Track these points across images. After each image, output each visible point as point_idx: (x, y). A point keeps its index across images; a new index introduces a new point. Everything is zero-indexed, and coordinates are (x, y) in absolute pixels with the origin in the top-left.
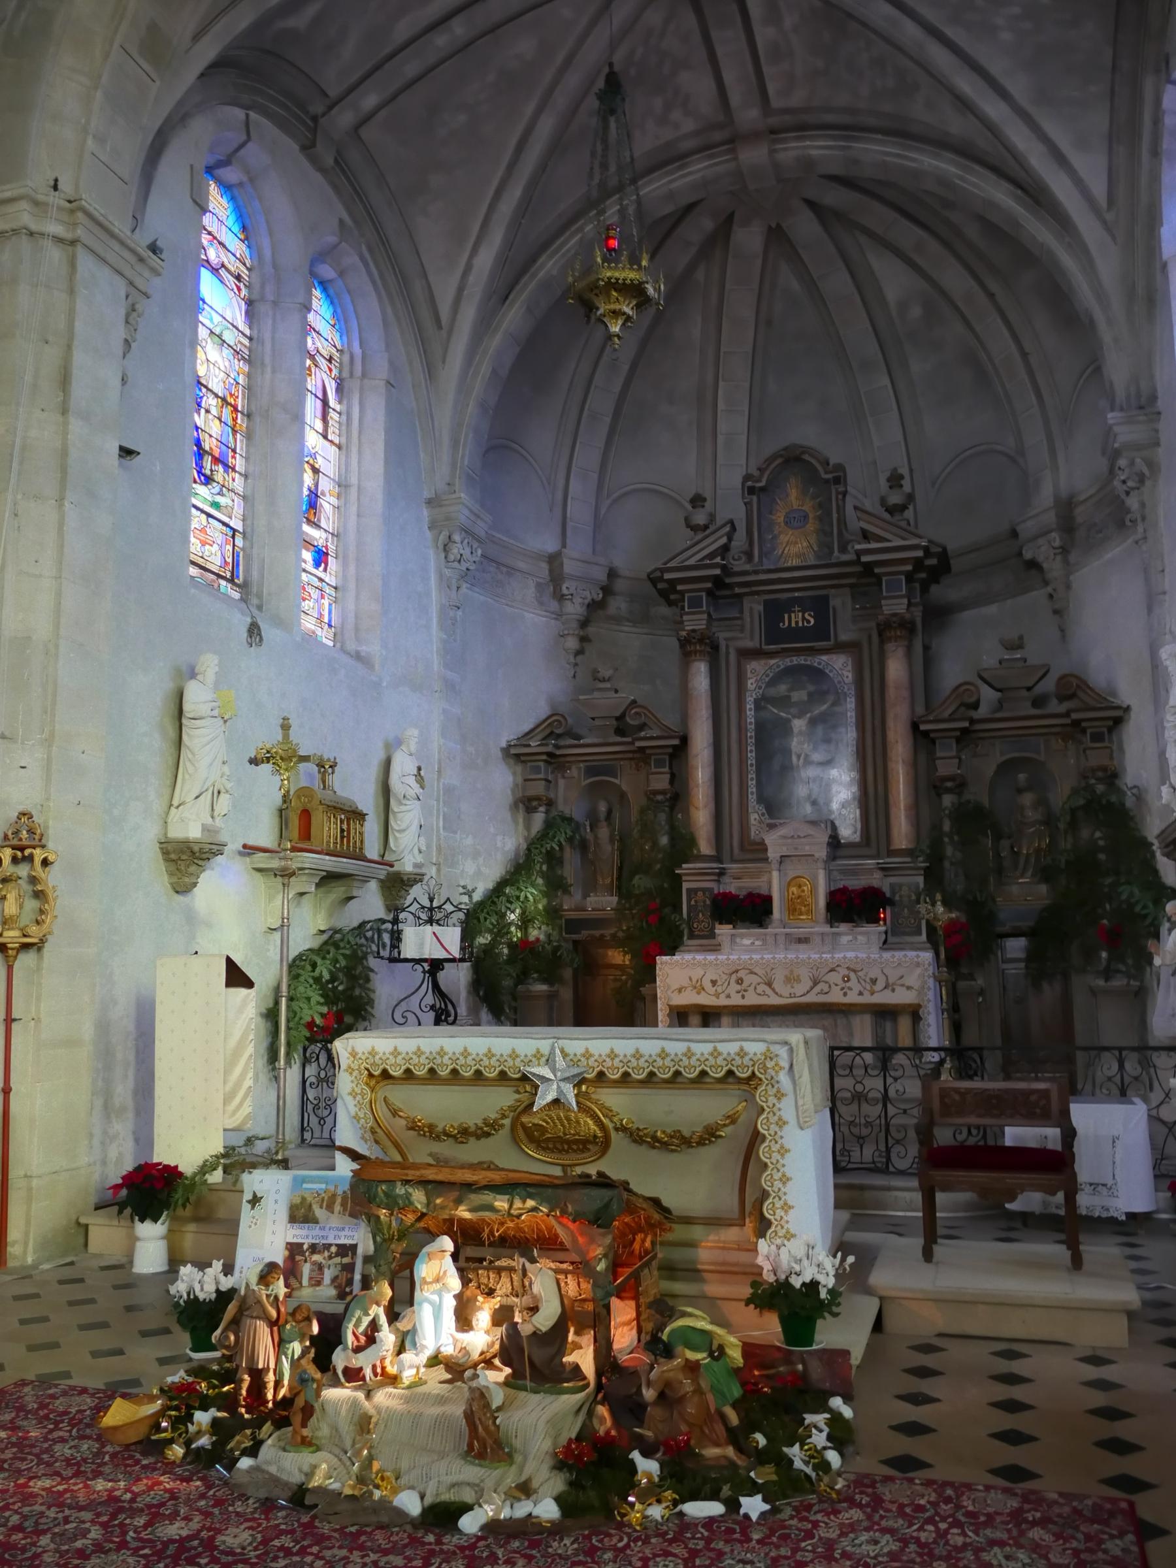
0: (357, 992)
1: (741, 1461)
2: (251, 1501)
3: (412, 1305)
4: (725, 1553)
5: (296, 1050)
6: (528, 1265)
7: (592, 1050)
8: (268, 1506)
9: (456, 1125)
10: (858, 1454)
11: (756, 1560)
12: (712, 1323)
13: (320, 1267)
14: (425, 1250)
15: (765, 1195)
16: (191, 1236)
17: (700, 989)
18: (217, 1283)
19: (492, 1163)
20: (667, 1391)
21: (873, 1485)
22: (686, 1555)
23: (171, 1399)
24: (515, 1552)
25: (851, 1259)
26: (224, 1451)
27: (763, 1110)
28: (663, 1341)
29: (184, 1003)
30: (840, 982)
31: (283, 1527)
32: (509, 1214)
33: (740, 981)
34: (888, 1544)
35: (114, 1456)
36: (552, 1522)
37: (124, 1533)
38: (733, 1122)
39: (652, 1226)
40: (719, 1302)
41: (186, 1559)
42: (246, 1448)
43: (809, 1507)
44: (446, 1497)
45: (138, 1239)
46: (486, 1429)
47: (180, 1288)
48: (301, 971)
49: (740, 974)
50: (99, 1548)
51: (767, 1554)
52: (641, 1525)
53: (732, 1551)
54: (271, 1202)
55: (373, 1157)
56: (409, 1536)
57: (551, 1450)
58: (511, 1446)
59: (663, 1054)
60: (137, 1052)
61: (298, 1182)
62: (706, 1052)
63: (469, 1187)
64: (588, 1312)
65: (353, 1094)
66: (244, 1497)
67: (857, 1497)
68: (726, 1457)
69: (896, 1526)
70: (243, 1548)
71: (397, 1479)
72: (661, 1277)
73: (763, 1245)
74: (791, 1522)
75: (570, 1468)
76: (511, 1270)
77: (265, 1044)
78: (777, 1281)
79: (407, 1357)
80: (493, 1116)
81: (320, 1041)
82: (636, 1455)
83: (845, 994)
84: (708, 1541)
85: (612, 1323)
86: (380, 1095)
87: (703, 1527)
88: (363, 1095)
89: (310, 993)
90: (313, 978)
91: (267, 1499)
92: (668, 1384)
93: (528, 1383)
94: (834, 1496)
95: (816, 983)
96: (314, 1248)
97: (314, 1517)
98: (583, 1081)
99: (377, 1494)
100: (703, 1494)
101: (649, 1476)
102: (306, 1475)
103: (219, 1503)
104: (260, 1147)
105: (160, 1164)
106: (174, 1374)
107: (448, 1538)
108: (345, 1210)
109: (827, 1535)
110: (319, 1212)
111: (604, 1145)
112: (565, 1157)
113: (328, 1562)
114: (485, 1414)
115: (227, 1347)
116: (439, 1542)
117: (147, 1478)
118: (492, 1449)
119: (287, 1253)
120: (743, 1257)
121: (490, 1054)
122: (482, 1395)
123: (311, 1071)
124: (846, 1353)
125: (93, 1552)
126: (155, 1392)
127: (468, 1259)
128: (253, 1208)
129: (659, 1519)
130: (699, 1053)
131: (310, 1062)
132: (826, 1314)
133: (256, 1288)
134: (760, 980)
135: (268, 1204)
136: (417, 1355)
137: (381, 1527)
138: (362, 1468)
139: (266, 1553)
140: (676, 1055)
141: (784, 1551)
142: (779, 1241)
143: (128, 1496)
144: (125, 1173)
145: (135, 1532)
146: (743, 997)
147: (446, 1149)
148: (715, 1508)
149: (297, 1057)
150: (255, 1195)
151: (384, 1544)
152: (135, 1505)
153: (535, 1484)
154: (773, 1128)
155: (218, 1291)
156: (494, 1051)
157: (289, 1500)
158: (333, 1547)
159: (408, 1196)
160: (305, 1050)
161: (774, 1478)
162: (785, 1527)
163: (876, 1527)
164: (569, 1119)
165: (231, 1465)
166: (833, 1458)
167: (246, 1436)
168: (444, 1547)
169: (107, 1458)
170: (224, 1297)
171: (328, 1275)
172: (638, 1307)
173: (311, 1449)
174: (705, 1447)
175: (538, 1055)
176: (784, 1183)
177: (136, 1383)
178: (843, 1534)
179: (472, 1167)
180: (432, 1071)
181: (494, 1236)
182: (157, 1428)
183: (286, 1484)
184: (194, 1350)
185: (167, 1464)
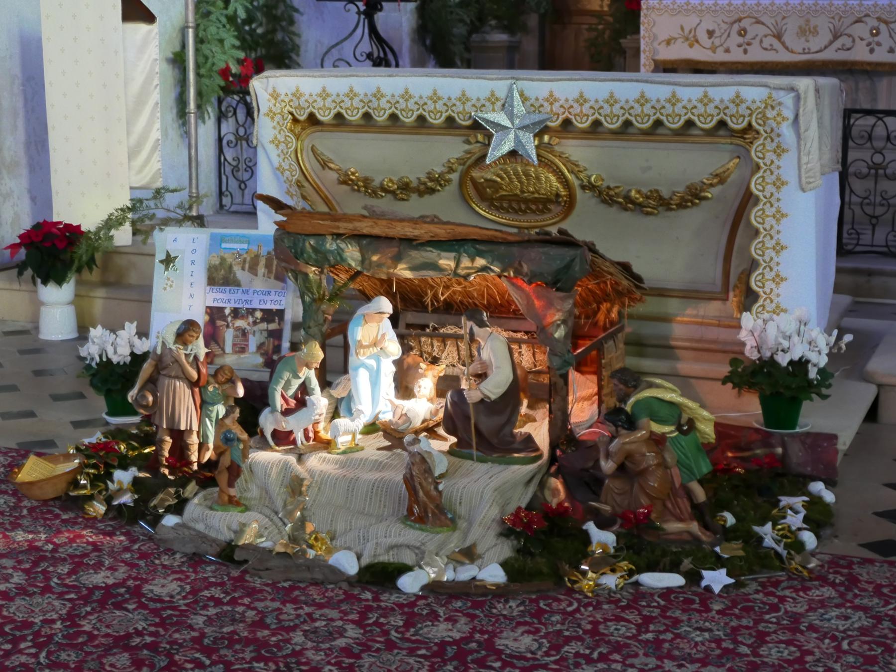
0: (279, 36)
1: (705, 537)
2: (178, 556)
3: (345, 371)
4: (682, 621)
5: (208, 101)
6: (476, 329)
7: (557, 94)
8: (196, 560)
9: (395, 179)
10: (836, 537)
11: (715, 628)
12: (682, 395)
13: (244, 333)
14: (360, 312)
15: (754, 264)
16: (99, 300)
17: (694, 41)
18: (132, 346)
19: (435, 217)
20: (627, 463)
21: (850, 566)
22: (640, 621)
23: (88, 457)
24: (457, 611)
25: (848, 338)
26: (147, 508)
27: (758, 168)
28: (626, 413)
29: (75, 39)
30: (867, 35)
31: (213, 580)
32: (455, 274)
33: (742, 33)
34: (859, 620)
35: (31, 510)
36: (498, 586)
37: (48, 579)
38: (722, 182)
39: (620, 295)
40: (693, 381)
41: (113, 604)
42: (170, 506)
43: (776, 584)
44: (384, 558)
45: (42, 304)
46: (427, 494)
47: (91, 350)
48: (212, 9)
49: (743, 24)
50: (22, 591)
51: (726, 624)
52: (592, 592)
53: (690, 619)
54: (187, 263)
55: (299, 208)
56: (345, 593)
57: (498, 518)
58: (455, 512)
59: (643, 100)
60: (26, 100)
61: (216, 241)
62: (694, 99)
63: (409, 242)
64: (544, 385)
65: (275, 142)
66: (170, 552)
67: (831, 577)
68: (689, 533)
69: (870, 604)
70: (172, 597)
71: (332, 539)
72: (628, 353)
73: (747, 320)
74: (756, 596)
75: (518, 536)
76: (457, 337)
77: (172, 95)
78: (759, 359)
79: (342, 422)
80: (439, 169)
81: (237, 93)
82: (590, 526)
83: (872, 51)
84: (664, 610)
85: (570, 398)
86: (307, 143)
87: (659, 597)
88: (286, 143)
89: (223, 34)
90: (226, 16)
91: (194, 554)
92: (629, 456)
93: (475, 452)
94: (805, 573)
95: (836, 37)
96: (236, 313)
97: (245, 572)
98: (545, 130)
99: (311, 553)
100: (662, 565)
101: (604, 546)
102: (235, 532)
103: (143, 556)
104: (171, 200)
105: (60, 223)
106: (91, 436)
107: (384, 597)
108: (270, 271)
109: (795, 610)
110: (241, 275)
111: (570, 205)
112: (522, 218)
113: (260, 612)
114: (426, 479)
115: (146, 407)
116: (376, 599)
117: (68, 531)
118: (434, 513)
119: (207, 318)
120: (724, 334)
121: (435, 97)
122: (423, 460)
123: (228, 127)
124: (832, 438)
125: (17, 594)
126: (71, 452)
127: (409, 326)
128: (167, 269)
129: (613, 587)
130: (686, 99)
131: (226, 117)
132: (814, 396)
133: (173, 348)
134: (770, 32)
135: (183, 263)
136: (353, 421)
137: (315, 583)
138: (294, 529)
139: (196, 602)
140: (658, 101)
141: (744, 622)
142: (766, 316)
143: (50, 547)
144: (22, 232)
145: (59, 578)
146: (745, 52)
147: (384, 204)
148: (675, 580)
149: (211, 112)
150: (168, 255)
151: (318, 598)
152: (57, 555)
153: (479, 550)
154: (770, 189)
155: (132, 354)
156: (440, 93)
157: (218, 556)
158: (266, 599)
159: (340, 252)
160: (220, 101)
161: (741, 553)
162: (749, 601)
163: (848, 604)
164: (527, 175)
165: (155, 520)
166: (809, 539)
167: (169, 494)
168: (382, 604)
169: (25, 512)
170: (138, 359)
171: (253, 342)
172: (600, 381)
173: (240, 509)
174: (667, 521)
175: (492, 99)
176: (778, 252)
177: (51, 444)
178: (811, 609)
179: (414, 221)
180: (367, 116)
181: (438, 301)
182: (76, 484)
183: (214, 541)
184: (111, 413)
185: (88, 519)
